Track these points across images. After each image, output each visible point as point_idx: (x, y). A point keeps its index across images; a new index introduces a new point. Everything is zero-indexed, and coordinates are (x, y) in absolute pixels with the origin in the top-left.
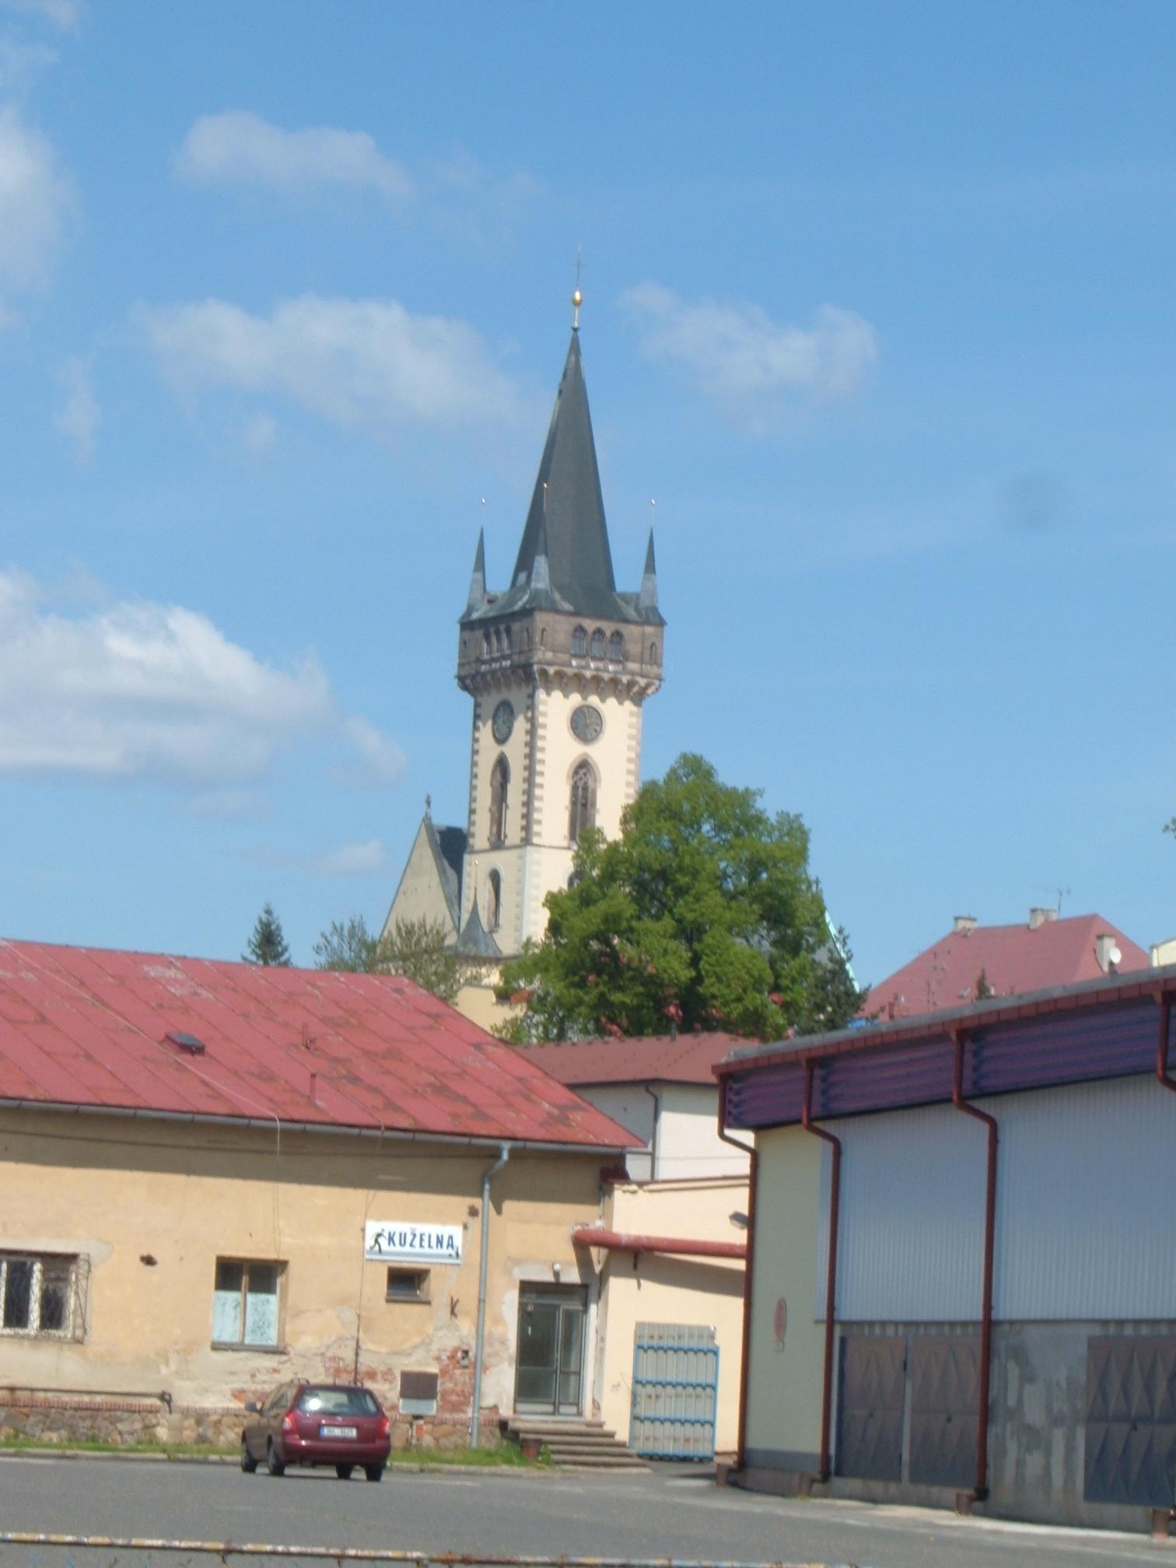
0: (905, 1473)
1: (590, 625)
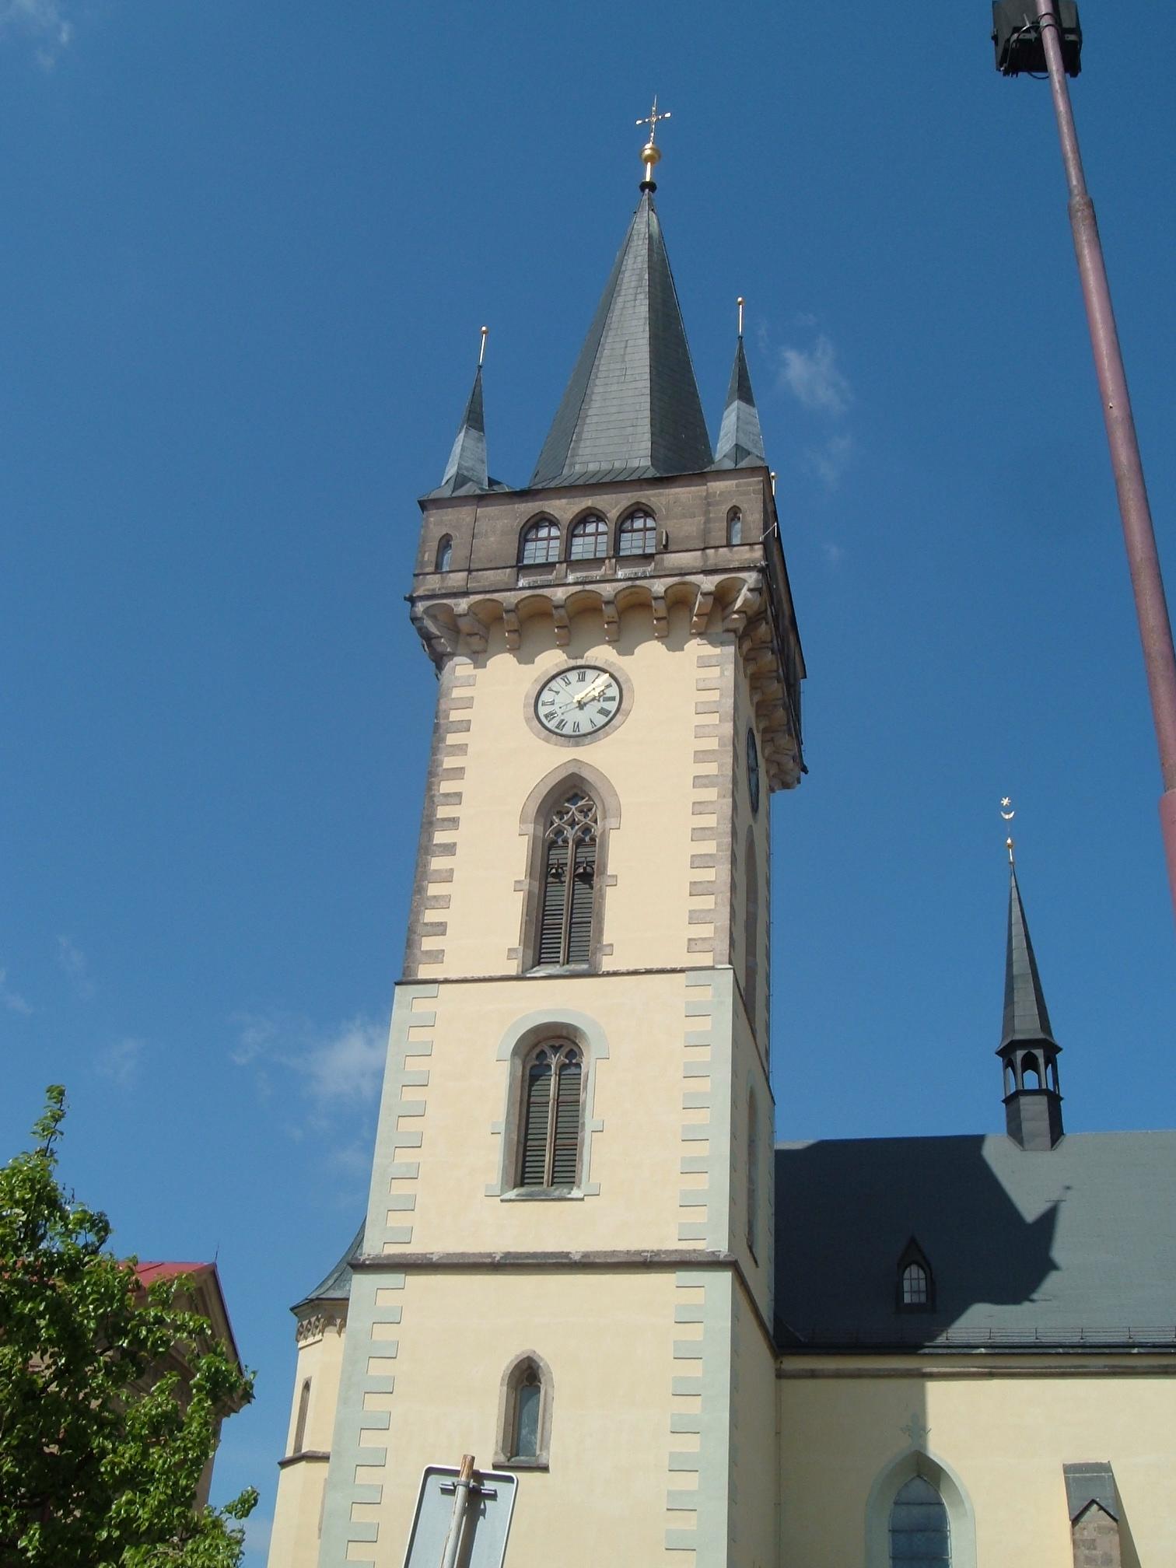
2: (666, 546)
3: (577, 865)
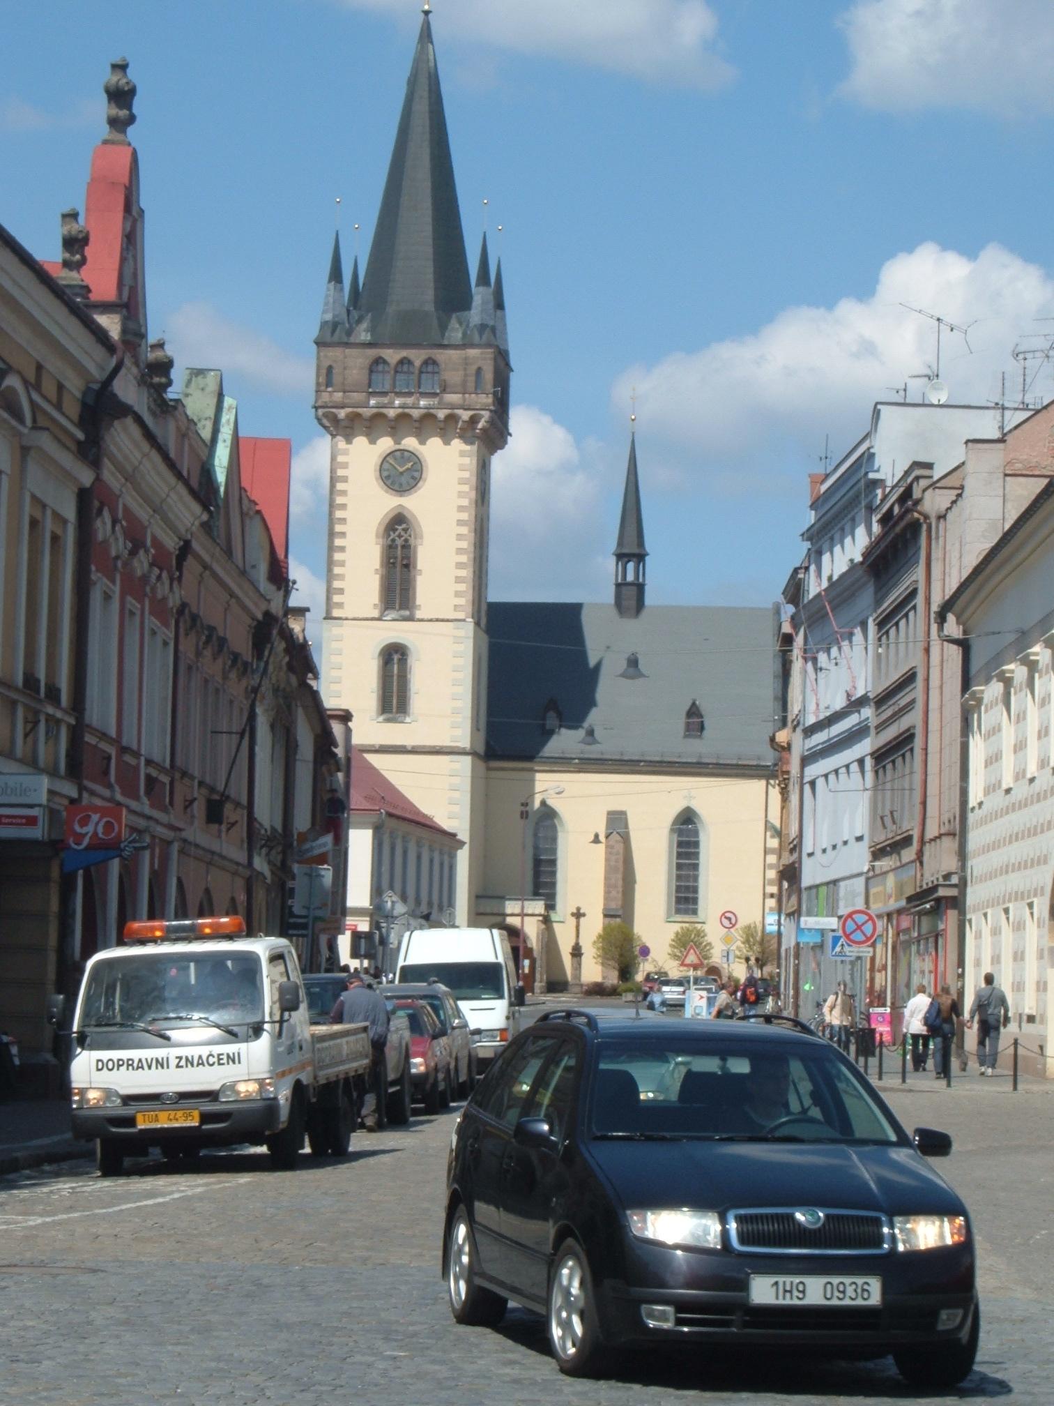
1: (392, 356)
2: (444, 390)
3: (403, 559)
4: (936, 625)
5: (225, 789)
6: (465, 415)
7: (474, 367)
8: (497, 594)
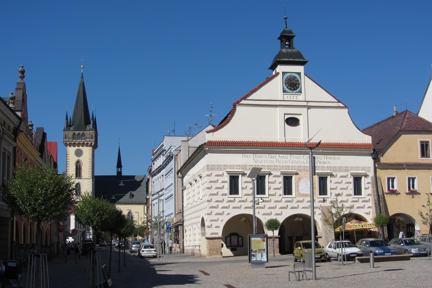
0: (412, 238)
1: (77, 132)
3: (79, 168)
4: (177, 175)
5: (64, 222)
6: (90, 143)
7: (91, 134)
8: (96, 174)
